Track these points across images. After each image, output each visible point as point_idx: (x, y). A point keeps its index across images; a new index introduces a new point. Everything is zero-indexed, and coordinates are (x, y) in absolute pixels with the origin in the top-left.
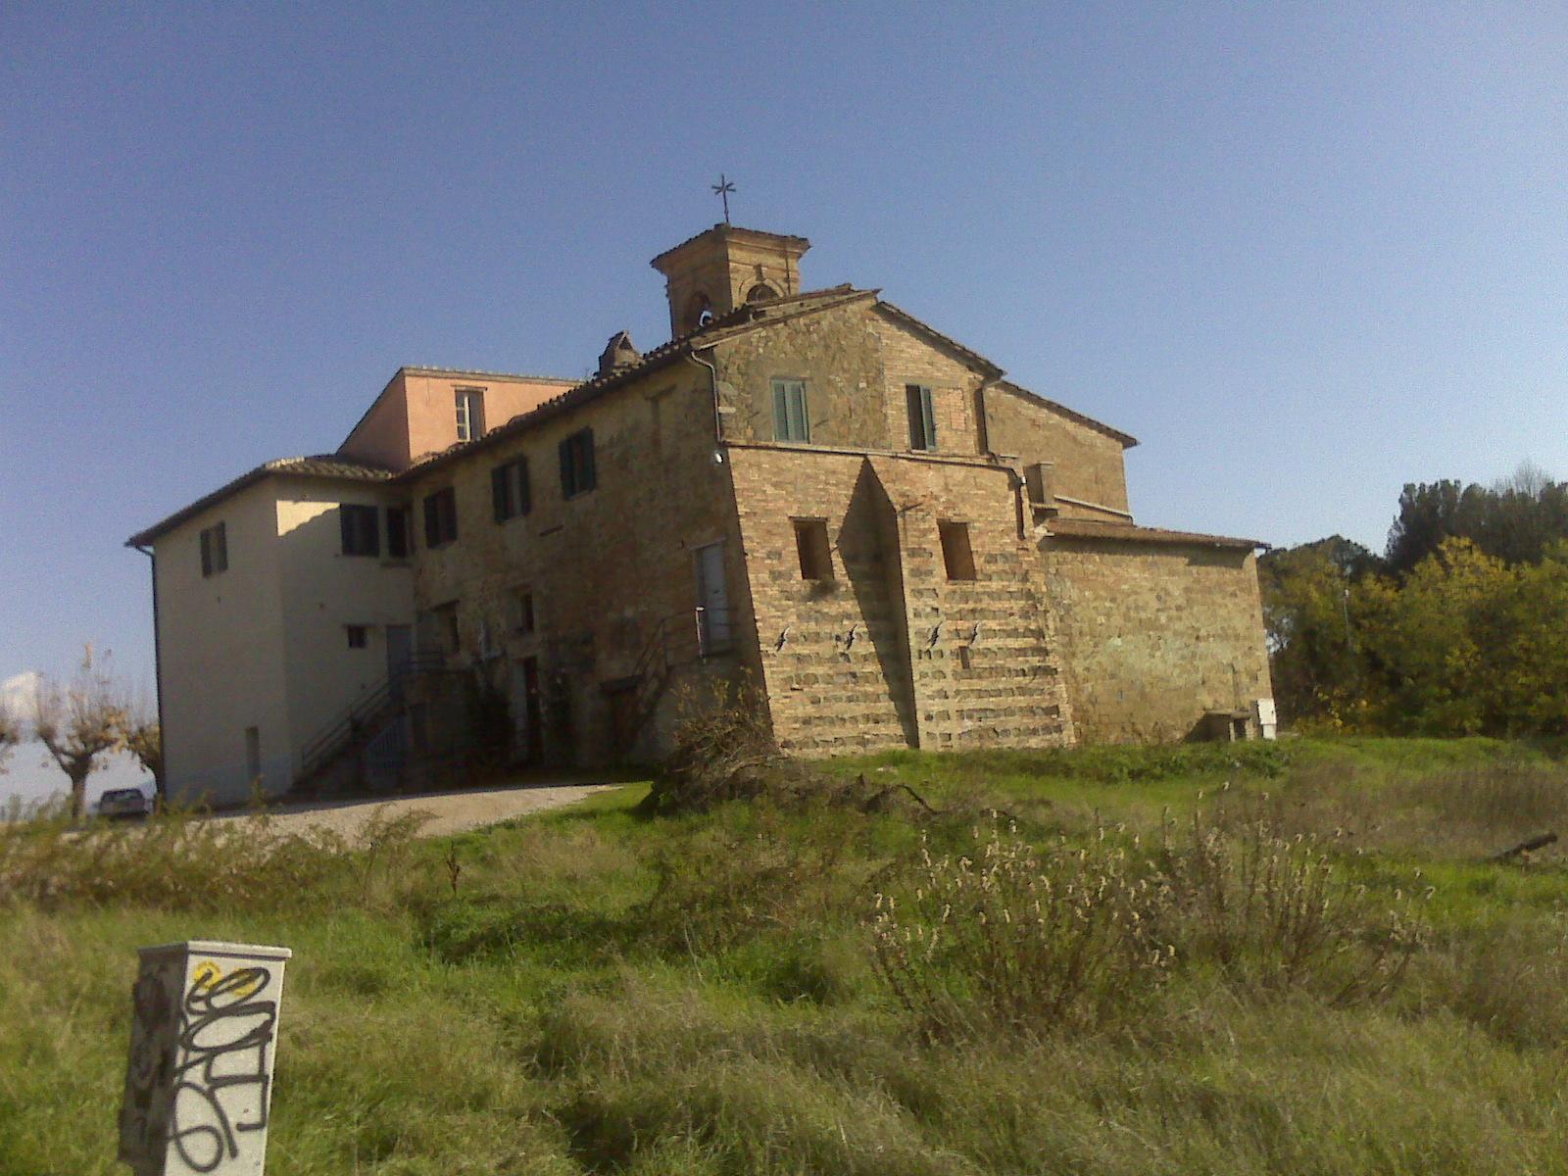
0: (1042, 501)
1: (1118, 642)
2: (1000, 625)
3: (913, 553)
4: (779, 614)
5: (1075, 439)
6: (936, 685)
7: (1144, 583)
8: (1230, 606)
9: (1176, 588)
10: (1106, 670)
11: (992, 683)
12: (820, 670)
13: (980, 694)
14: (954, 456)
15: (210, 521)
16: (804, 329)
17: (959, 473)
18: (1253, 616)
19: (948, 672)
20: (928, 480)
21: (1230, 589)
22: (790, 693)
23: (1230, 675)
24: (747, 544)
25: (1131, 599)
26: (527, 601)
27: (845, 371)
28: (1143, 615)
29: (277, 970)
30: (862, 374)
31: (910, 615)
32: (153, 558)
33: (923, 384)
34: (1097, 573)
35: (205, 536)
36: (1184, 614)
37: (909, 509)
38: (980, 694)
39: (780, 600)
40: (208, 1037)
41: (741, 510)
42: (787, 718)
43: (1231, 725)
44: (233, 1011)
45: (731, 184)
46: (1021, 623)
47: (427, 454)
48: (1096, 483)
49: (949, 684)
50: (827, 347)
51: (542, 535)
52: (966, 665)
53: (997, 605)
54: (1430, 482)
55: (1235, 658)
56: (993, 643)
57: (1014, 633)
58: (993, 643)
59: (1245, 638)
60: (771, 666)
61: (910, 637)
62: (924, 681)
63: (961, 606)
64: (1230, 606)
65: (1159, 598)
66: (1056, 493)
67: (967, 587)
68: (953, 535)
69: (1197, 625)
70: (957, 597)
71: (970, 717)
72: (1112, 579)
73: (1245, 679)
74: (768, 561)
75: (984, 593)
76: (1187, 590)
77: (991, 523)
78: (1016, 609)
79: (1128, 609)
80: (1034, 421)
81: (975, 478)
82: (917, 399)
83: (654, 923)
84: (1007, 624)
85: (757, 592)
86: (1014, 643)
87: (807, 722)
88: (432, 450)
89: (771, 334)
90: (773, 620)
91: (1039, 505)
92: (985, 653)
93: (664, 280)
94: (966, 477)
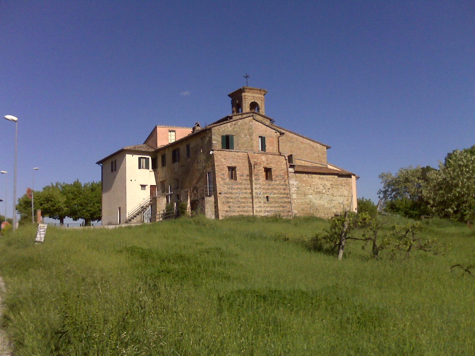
0: (292, 163)
1: (311, 196)
3: (256, 175)
5: (313, 147)
6: (259, 205)
9: (328, 184)
12: (231, 200)
13: (271, 207)
15: (113, 159)
17: (271, 156)
21: (344, 185)
22: (224, 205)
25: (316, 186)
26: (178, 181)
27: (244, 133)
28: (318, 190)
29: (46, 226)
33: (263, 136)
35: (112, 163)
38: (271, 207)
40: (40, 231)
41: (216, 164)
44: (42, 229)
46: (282, 191)
47: (161, 146)
48: (318, 157)
52: (268, 200)
53: (278, 187)
54: (22, 196)
55: (344, 201)
56: (275, 196)
57: (281, 194)
58: (275, 196)
59: (347, 197)
62: (256, 203)
64: (343, 189)
65: (323, 186)
66: (296, 162)
68: (268, 171)
70: (267, 185)
72: (311, 181)
74: (221, 176)
75: (274, 184)
76: (331, 185)
77: (278, 168)
79: (314, 188)
82: (263, 139)
84: (280, 191)
86: (282, 196)
87: (227, 211)
88: (163, 144)
91: (291, 164)
92: (273, 198)
93: (231, 99)
94: (272, 158)
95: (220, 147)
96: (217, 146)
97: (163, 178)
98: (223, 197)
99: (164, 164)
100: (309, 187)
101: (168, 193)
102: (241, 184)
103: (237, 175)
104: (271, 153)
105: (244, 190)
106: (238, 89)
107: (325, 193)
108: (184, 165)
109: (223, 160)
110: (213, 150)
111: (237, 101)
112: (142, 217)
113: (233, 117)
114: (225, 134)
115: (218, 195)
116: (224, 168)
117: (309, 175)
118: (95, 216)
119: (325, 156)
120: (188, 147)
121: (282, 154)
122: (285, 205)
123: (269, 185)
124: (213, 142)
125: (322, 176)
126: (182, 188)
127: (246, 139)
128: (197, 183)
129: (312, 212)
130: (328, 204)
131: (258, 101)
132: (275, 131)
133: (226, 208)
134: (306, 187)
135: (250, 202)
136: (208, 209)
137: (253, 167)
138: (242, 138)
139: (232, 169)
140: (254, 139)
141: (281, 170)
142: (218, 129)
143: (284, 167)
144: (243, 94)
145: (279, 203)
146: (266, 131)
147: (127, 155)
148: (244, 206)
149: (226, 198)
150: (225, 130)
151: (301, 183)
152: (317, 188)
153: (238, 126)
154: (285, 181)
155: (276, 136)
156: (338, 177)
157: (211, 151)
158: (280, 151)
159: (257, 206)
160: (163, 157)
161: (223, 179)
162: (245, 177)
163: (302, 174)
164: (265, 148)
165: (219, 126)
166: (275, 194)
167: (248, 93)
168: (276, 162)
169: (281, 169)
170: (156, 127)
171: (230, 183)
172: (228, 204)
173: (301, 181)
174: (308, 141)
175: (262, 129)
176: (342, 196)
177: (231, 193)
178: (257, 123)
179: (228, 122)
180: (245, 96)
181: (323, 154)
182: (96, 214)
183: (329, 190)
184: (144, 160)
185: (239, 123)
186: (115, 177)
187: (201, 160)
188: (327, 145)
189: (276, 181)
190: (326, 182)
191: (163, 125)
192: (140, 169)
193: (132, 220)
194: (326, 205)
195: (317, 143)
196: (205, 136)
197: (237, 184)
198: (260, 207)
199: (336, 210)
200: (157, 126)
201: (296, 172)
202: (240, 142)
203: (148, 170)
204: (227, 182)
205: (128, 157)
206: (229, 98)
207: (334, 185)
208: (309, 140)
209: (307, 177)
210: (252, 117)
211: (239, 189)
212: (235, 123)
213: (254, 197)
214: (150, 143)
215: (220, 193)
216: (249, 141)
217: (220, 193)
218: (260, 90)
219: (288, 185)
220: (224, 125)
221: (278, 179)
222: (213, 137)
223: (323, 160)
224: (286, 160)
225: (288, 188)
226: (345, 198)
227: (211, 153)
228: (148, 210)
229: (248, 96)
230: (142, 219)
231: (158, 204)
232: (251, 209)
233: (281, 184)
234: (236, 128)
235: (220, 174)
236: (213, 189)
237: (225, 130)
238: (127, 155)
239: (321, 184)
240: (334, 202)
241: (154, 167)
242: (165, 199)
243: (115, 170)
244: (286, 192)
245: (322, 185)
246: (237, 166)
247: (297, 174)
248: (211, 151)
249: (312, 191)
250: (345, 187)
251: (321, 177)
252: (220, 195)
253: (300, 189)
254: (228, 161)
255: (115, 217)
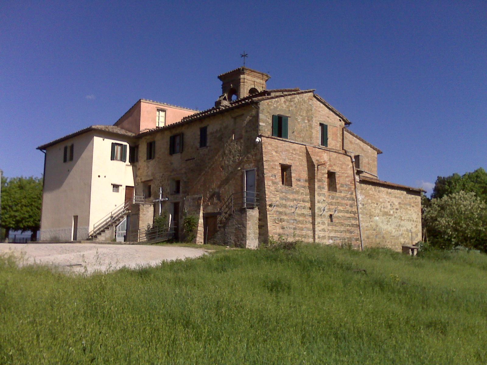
0: (359, 168)
2: (343, 208)
3: (319, 181)
4: (274, 196)
6: (323, 227)
7: (387, 199)
8: (412, 210)
9: (396, 202)
10: (373, 227)
11: (339, 228)
12: (285, 218)
13: (336, 231)
14: (334, 149)
15: (69, 144)
16: (289, 99)
17: (335, 155)
18: (418, 214)
19: (326, 222)
20: (325, 157)
21: (412, 204)
22: (275, 224)
23: (410, 234)
24: (265, 171)
25: (383, 204)
27: (301, 116)
28: (386, 210)
30: (306, 118)
31: (316, 202)
32: (45, 154)
33: (325, 123)
34: (373, 195)
35: (66, 149)
36: (398, 211)
37: (319, 165)
39: (274, 191)
41: (264, 159)
42: (273, 233)
43: (410, 250)
45: (247, 55)
46: (348, 208)
47: (146, 129)
49: (325, 227)
50: (296, 107)
51: (186, 160)
52: (332, 221)
53: (344, 202)
55: (412, 228)
56: (341, 214)
57: (347, 212)
58: (341, 214)
60: (270, 214)
61: (316, 209)
62: (319, 225)
63: (331, 200)
65: (391, 205)
67: (334, 194)
68: (331, 175)
69: (401, 216)
70: (330, 198)
71: (332, 239)
72: (377, 197)
73: (414, 235)
74: (271, 178)
75: (339, 197)
76: (400, 203)
78: (348, 203)
79: (381, 207)
80: (351, 141)
81: (339, 157)
82: (324, 128)
83: (401, 329)
85: (267, 188)
86: (348, 215)
89: (279, 100)
90: (271, 198)
91: (359, 169)
92: (338, 217)
93: (221, 83)
95: (269, 133)
96: (266, 130)
97: (147, 176)
98: (274, 211)
99: (150, 156)
100: (375, 205)
101: (159, 199)
102: (297, 192)
103: (293, 179)
104: (334, 151)
105: (301, 202)
106: (236, 68)
107: (392, 215)
108: (194, 159)
109: (274, 153)
110: (260, 136)
111: (232, 85)
112: (112, 233)
113: (272, 94)
114: (277, 113)
115: (268, 207)
116: (275, 165)
117: (376, 187)
118: (21, 225)
119: (376, 163)
120: (203, 131)
121: (348, 154)
122: (353, 229)
123: (333, 198)
124: (261, 124)
125: (390, 190)
126: (186, 193)
127: (304, 125)
128: (220, 187)
129: (378, 240)
130: (395, 231)
131: (258, 87)
132: (339, 118)
133: (278, 230)
134: (372, 204)
135: (309, 221)
136: (250, 229)
137: (316, 169)
138: (299, 123)
139: (285, 169)
140: (313, 126)
141: (347, 177)
142: (268, 104)
143: (350, 172)
144: (242, 76)
145: (345, 226)
146: (329, 117)
147: (95, 138)
148: (302, 227)
149: (278, 213)
150: (277, 108)
151: (367, 198)
152: (384, 207)
153: (295, 104)
154: (352, 194)
155: (340, 126)
156: (407, 193)
157: (257, 138)
158: (344, 149)
159: (320, 228)
160: (151, 147)
161: (274, 183)
162: (302, 183)
163: (368, 186)
164: (327, 141)
165: (270, 100)
166: (340, 211)
167: (248, 75)
168: (341, 164)
169: (346, 175)
170: (139, 102)
171: (284, 190)
172: (280, 224)
173: (367, 195)
174: (358, 141)
175: (323, 113)
176: (411, 221)
177: (285, 206)
178: (319, 102)
179: (282, 96)
180: (244, 79)
181: (374, 161)
182: (24, 221)
183: (397, 211)
184: (119, 148)
185: (296, 100)
186: (69, 171)
187: (230, 152)
188: (378, 148)
189: (341, 192)
190: (394, 198)
191: (149, 101)
192: (113, 161)
193: (99, 237)
194: (394, 233)
195: (368, 144)
196: (243, 115)
197: (293, 193)
198: (324, 230)
199: (404, 240)
200: (141, 101)
201: (363, 182)
202: (296, 128)
203: (124, 163)
204: (280, 188)
205: (97, 141)
206: (219, 80)
207: (402, 204)
208: (359, 139)
209: (373, 189)
210: (311, 94)
211: (296, 200)
212: (291, 99)
213: (316, 215)
214: (126, 124)
215: (270, 206)
216: (308, 129)
217: (270, 206)
218: (263, 74)
219: (355, 200)
220: (276, 99)
221: (343, 190)
222: (261, 116)
223: (373, 169)
224: (352, 162)
225: (356, 204)
226: (414, 223)
227: (258, 140)
228: (122, 223)
229: (248, 80)
230: (113, 236)
231: (141, 215)
232: (310, 233)
233: (347, 198)
234: (292, 106)
235: (270, 174)
236: (256, 198)
237: (277, 108)
238: (95, 138)
239: (389, 202)
240: (402, 229)
241: (133, 160)
242: (152, 208)
243: (71, 159)
244: (353, 210)
245: (390, 204)
246: (293, 165)
247: (362, 185)
248: (257, 138)
249: (379, 211)
250: (414, 208)
251: (389, 192)
252: (270, 209)
253: (366, 207)
254: (281, 156)
255: (65, 230)
